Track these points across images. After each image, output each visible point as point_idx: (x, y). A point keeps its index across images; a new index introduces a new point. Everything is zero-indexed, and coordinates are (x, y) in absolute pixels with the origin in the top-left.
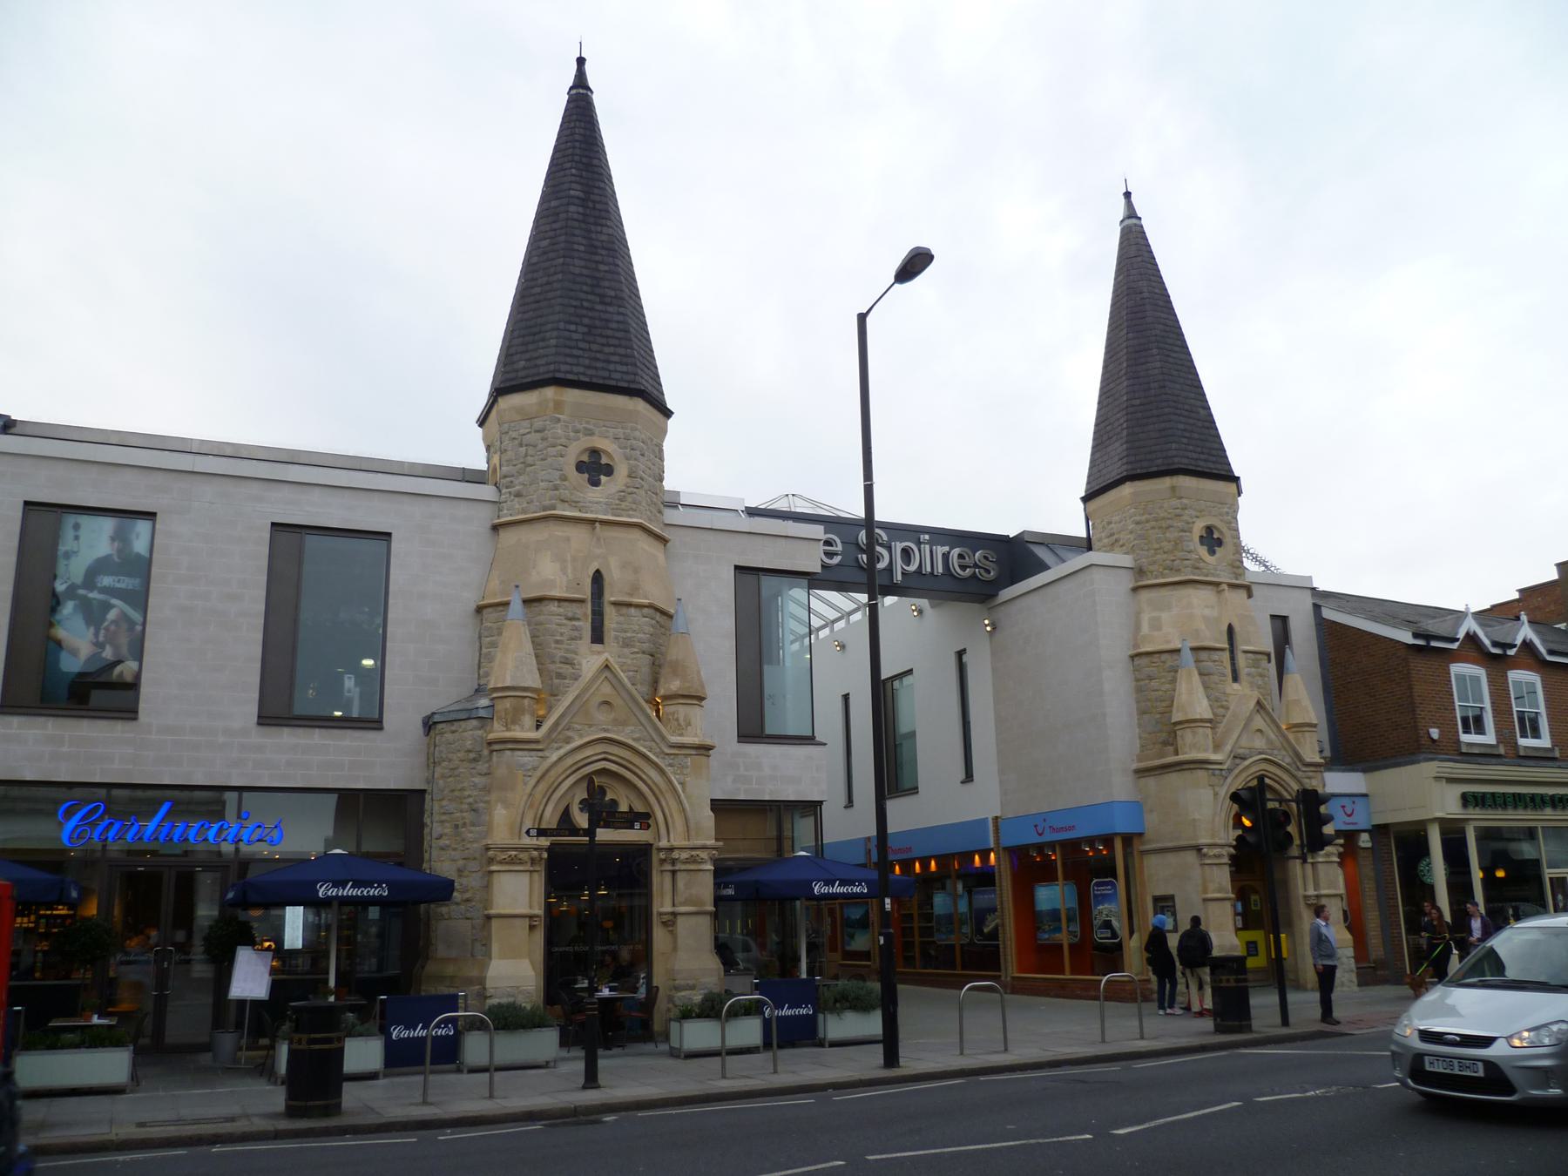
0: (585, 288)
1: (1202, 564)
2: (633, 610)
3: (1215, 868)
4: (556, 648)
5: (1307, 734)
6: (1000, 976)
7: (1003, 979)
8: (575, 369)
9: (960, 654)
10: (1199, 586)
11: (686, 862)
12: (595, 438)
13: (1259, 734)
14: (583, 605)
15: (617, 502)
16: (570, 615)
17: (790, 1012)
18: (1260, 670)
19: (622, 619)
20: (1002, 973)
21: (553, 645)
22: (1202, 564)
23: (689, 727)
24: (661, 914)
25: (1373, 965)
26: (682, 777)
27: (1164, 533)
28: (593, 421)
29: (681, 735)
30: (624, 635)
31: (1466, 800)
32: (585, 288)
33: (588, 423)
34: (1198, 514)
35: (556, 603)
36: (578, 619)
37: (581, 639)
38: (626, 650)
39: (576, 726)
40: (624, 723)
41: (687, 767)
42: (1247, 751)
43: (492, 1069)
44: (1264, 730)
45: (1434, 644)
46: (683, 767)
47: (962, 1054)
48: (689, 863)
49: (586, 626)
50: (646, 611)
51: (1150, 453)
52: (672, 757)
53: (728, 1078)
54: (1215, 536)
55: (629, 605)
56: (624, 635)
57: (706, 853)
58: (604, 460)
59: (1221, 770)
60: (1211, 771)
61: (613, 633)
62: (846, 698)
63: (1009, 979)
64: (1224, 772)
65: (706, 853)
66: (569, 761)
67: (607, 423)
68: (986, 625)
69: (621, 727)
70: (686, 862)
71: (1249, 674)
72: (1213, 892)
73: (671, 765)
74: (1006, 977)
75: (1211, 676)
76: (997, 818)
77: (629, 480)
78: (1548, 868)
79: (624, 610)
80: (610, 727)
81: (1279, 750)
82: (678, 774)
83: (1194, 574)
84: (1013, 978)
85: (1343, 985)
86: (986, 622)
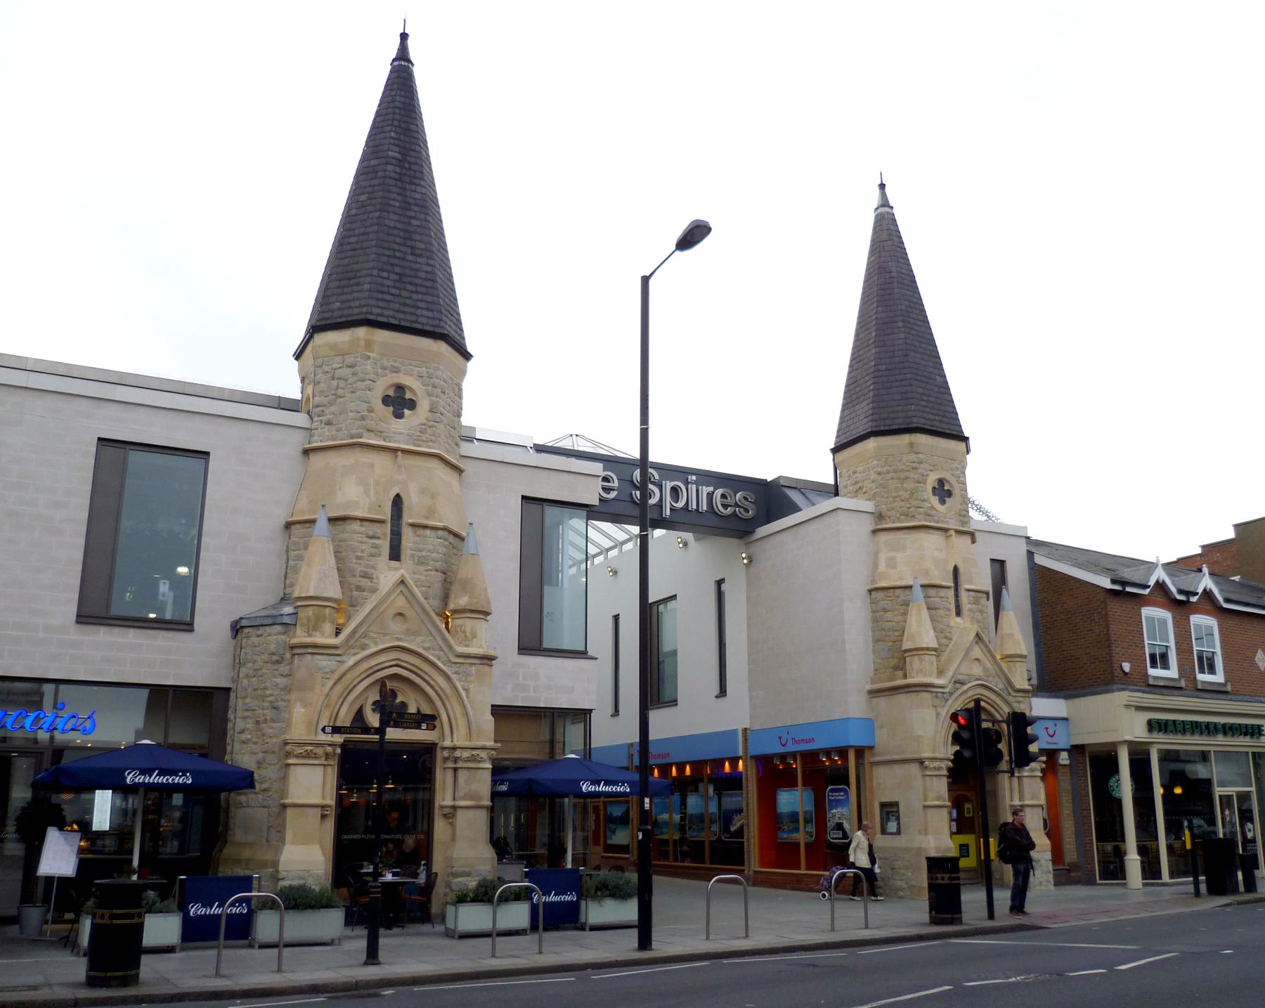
0: (398, 240)
1: (934, 512)
2: (428, 532)
3: (935, 779)
4: (356, 563)
5: (1018, 664)
6: (744, 870)
7: (746, 872)
8: (386, 312)
9: (719, 583)
10: (930, 531)
11: (468, 760)
12: (401, 375)
13: (399, 618)
14: (383, 525)
15: (418, 434)
16: (371, 533)
17: (557, 899)
18: (980, 606)
19: (418, 539)
20: (746, 868)
21: (354, 561)
22: (934, 512)
23: (475, 640)
24: (442, 807)
25: (1068, 867)
26: (466, 684)
27: (902, 484)
28: (399, 360)
29: (467, 646)
30: (419, 554)
31: (1152, 726)
32: (398, 240)
33: (395, 361)
34: (932, 468)
35: (359, 523)
36: (379, 538)
37: (380, 555)
38: (421, 568)
39: (371, 634)
40: (416, 634)
41: (471, 675)
42: (966, 678)
43: (494, 935)
44: (981, 658)
45: (1129, 589)
46: (468, 675)
47: (708, 938)
48: (470, 761)
49: (385, 545)
50: (440, 532)
51: (893, 412)
52: (458, 665)
53: (223, 976)
54: (946, 488)
55: (425, 527)
56: (419, 554)
57: (486, 753)
58: (408, 396)
59: (943, 693)
60: (934, 694)
61: (409, 552)
62: (616, 618)
63: (751, 873)
64: (945, 695)
65: (486, 753)
66: (365, 666)
67: (414, 363)
68: (743, 559)
69: (413, 637)
70: (468, 760)
71: (970, 610)
72: (932, 800)
73: (457, 673)
74: (749, 871)
75: (938, 611)
76: (746, 729)
77: (430, 414)
78: (1218, 786)
79: (420, 531)
80: (402, 636)
81: (994, 677)
82: (463, 681)
83: (926, 520)
84: (755, 872)
85: (1041, 884)
86: (744, 555)
